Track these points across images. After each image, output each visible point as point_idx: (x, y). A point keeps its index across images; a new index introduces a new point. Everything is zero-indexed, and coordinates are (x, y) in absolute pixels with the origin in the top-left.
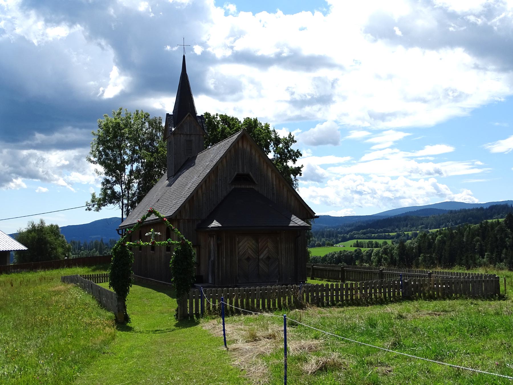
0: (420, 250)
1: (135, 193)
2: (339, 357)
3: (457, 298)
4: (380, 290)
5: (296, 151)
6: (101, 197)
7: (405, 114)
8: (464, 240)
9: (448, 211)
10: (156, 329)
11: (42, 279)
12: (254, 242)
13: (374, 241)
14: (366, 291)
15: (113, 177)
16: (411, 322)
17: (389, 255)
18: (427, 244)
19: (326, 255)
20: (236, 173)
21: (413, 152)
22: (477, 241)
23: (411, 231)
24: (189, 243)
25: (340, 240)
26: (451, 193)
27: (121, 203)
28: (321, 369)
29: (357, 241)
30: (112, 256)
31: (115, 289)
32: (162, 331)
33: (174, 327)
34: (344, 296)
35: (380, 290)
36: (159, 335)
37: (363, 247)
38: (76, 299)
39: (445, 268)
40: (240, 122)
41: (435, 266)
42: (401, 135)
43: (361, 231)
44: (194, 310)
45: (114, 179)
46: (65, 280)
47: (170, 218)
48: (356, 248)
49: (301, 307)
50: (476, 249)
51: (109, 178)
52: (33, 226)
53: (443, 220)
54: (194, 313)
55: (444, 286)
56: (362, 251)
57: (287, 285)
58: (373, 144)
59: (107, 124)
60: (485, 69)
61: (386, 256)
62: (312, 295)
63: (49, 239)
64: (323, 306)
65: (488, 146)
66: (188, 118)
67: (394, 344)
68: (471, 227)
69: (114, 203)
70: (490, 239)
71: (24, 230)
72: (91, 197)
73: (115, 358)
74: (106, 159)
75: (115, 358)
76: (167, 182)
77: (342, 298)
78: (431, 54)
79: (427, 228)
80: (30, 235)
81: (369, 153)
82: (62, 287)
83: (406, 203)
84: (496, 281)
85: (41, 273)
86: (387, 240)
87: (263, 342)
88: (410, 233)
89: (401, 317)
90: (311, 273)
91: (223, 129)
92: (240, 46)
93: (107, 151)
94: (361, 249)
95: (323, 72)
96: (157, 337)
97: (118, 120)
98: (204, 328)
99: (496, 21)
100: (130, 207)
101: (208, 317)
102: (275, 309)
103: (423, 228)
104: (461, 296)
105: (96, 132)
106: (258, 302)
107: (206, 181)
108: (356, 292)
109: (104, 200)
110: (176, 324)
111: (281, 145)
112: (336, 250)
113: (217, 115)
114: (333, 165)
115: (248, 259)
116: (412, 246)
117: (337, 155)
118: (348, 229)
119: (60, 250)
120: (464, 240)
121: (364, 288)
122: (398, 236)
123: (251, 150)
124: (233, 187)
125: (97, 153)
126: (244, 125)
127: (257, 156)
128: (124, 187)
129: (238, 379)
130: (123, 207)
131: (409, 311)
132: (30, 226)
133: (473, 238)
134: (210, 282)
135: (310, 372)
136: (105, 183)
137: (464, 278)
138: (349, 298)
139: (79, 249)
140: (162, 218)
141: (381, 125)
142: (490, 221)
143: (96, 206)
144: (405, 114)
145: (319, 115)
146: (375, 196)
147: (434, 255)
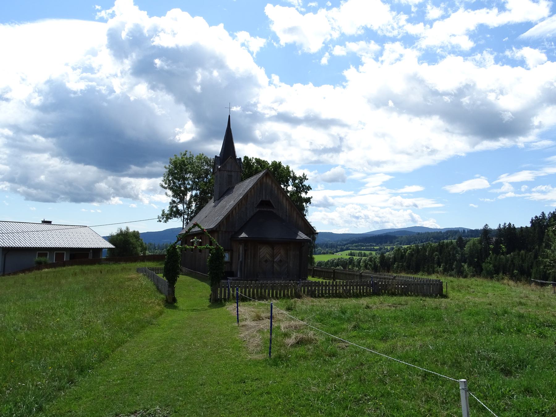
0: (395, 259)
1: (193, 211)
2: (314, 334)
3: (409, 295)
4: (357, 287)
5: (307, 186)
6: (168, 212)
7: (394, 163)
8: (427, 254)
9: (417, 233)
10: (194, 308)
11: (123, 270)
12: (270, 249)
13: (363, 252)
14: (346, 288)
15: (178, 199)
16: (374, 311)
17: (373, 262)
18: (400, 255)
19: (329, 261)
20: (260, 200)
21: (396, 190)
22: (436, 255)
23: (390, 246)
24: (222, 248)
25: (339, 250)
26: (421, 220)
27: (182, 217)
28: (298, 343)
29: (351, 252)
30: (166, 255)
31: (167, 279)
32: (198, 310)
33: (208, 308)
34: (331, 291)
35: (357, 287)
36: (195, 312)
37: (355, 256)
38: (142, 284)
39: (407, 273)
40: (269, 164)
41: (401, 272)
42: (387, 178)
43: (354, 244)
44: (223, 296)
45: (179, 200)
46: (139, 270)
47: (211, 231)
48: (350, 256)
49: (299, 297)
50: (435, 261)
51: (175, 200)
52: (121, 231)
53: (412, 239)
54: (223, 298)
55: (403, 286)
56: (354, 258)
57: (290, 281)
58: (367, 183)
59: (176, 161)
60: (452, 133)
61: (371, 263)
62: (308, 289)
63: (132, 241)
64: (315, 297)
65: (448, 188)
66: (230, 159)
67: (355, 327)
68: (432, 245)
69: (177, 217)
70: (445, 254)
71: (115, 234)
72: (162, 213)
73: (159, 328)
74: (173, 186)
75: (159, 328)
76: (213, 204)
77: (329, 292)
78: (417, 120)
79: (401, 244)
80: (119, 238)
81: (365, 188)
82: (134, 275)
83: (389, 226)
84: (440, 285)
85: (123, 265)
86: (372, 252)
87: (264, 321)
88: (389, 247)
89: (368, 307)
90: (312, 273)
91: (257, 168)
92: (282, 109)
93: (175, 180)
94: (354, 257)
95: (335, 130)
96: (193, 314)
97: (184, 159)
98: (228, 309)
99: (466, 100)
100: (189, 221)
101: (232, 301)
102: (280, 297)
103: (399, 244)
104: (414, 294)
105: (167, 166)
106: (269, 292)
107: (239, 205)
108: (340, 288)
109: (171, 215)
110: (209, 305)
111: (297, 181)
112: (336, 257)
113: (253, 158)
114: (339, 197)
115: (266, 261)
116: (390, 256)
117: (345, 190)
118: (345, 243)
119: (139, 249)
120: (427, 254)
121: (345, 285)
122: (380, 249)
123: (272, 183)
124: (258, 210)
125: (168, 181)
126: (271, 166)
127: (276, 189)
128: (185, 206)
129: (240, 347)
130: (184, 220)
131: (375, 304)
132: (119, 231)
133: (433, 253)
134: (239, 276)
135: (290, 344)
136: (172, 203)
137: (421, 281)
138: (334, 292)
139: (154, 249)
140: (203, 230)
141: (375, 169)
142: (445, 241)
143: (165, 219)
144: (394, 163)
145: (332, 161)
146: (368, 220)
147: (405, 264)
